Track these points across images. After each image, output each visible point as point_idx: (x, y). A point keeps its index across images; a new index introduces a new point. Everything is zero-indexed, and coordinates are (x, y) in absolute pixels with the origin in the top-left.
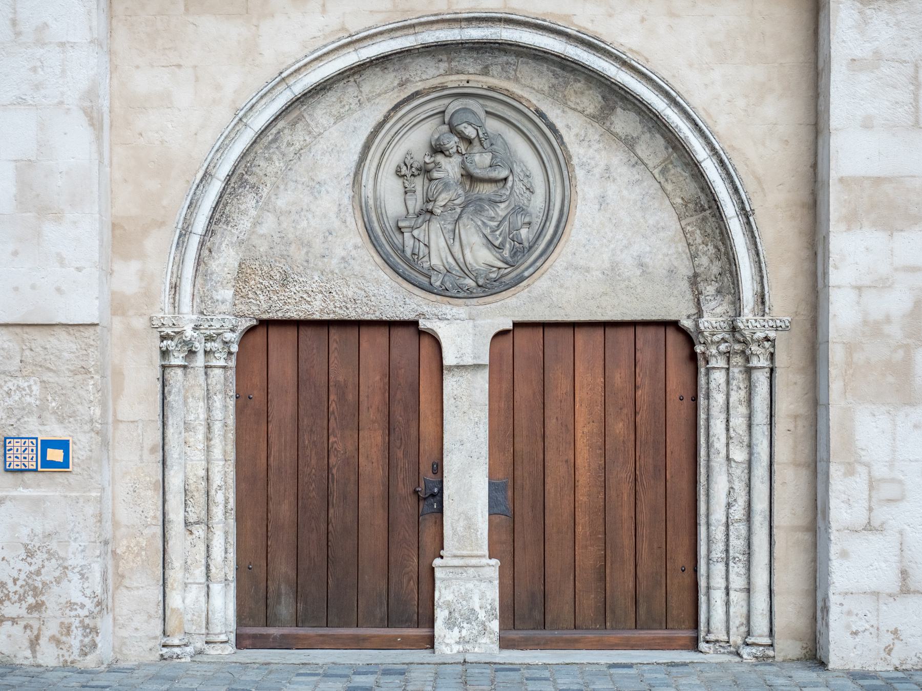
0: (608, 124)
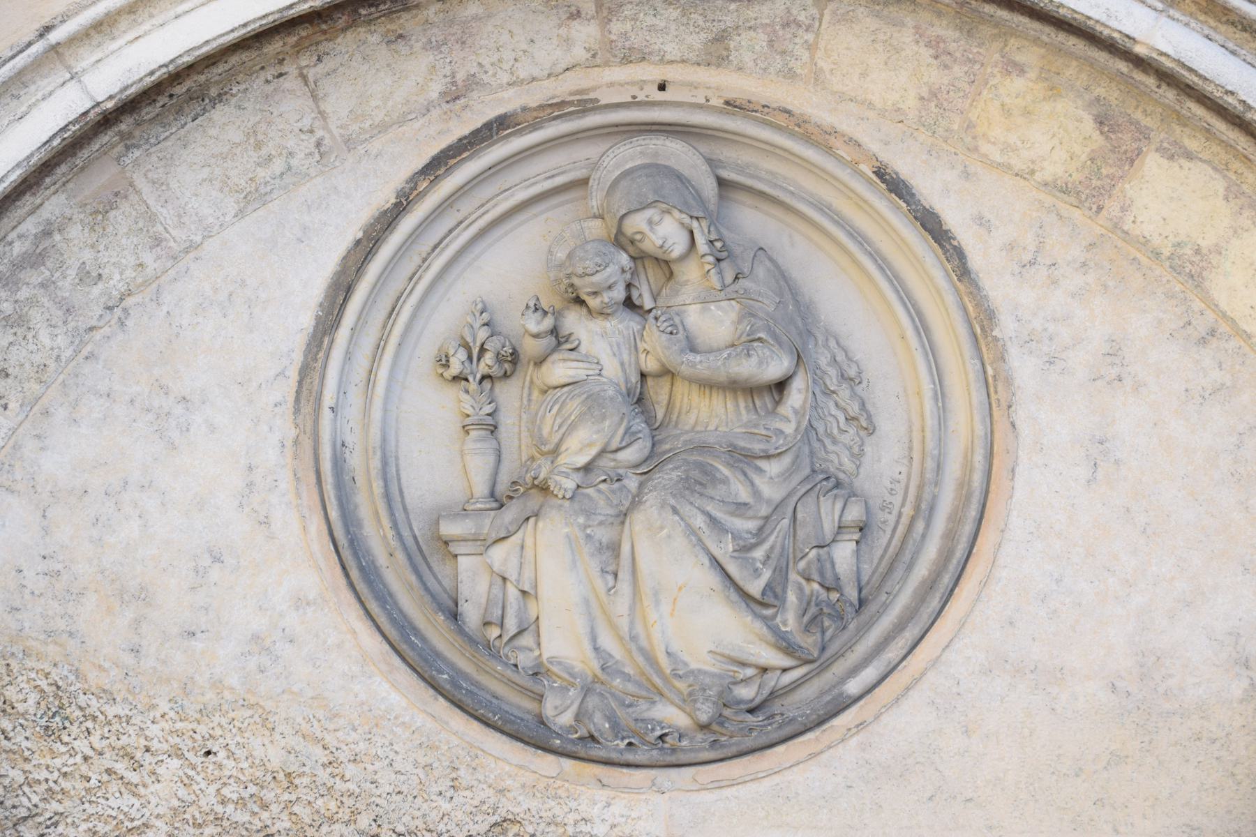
0: (1112, 208)
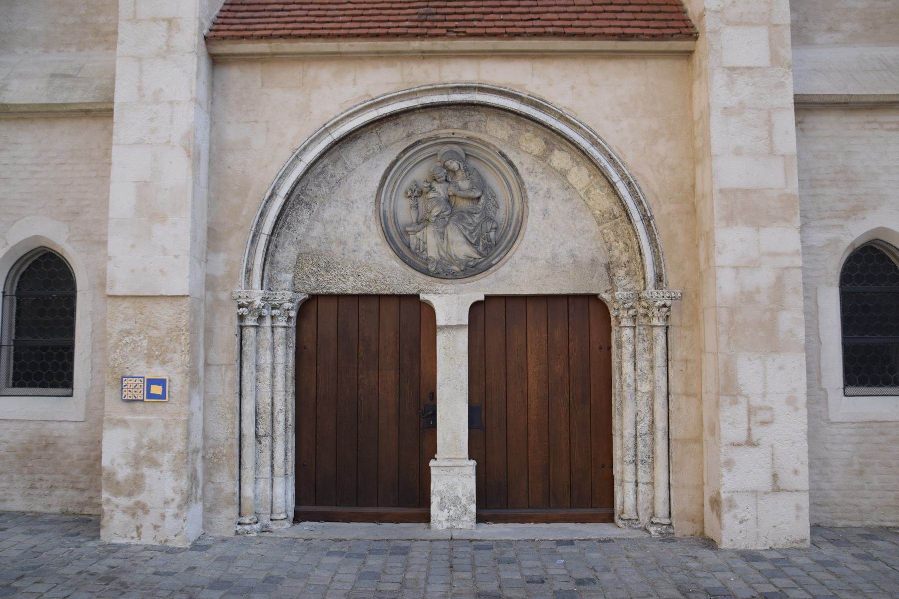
0: (548, 161)
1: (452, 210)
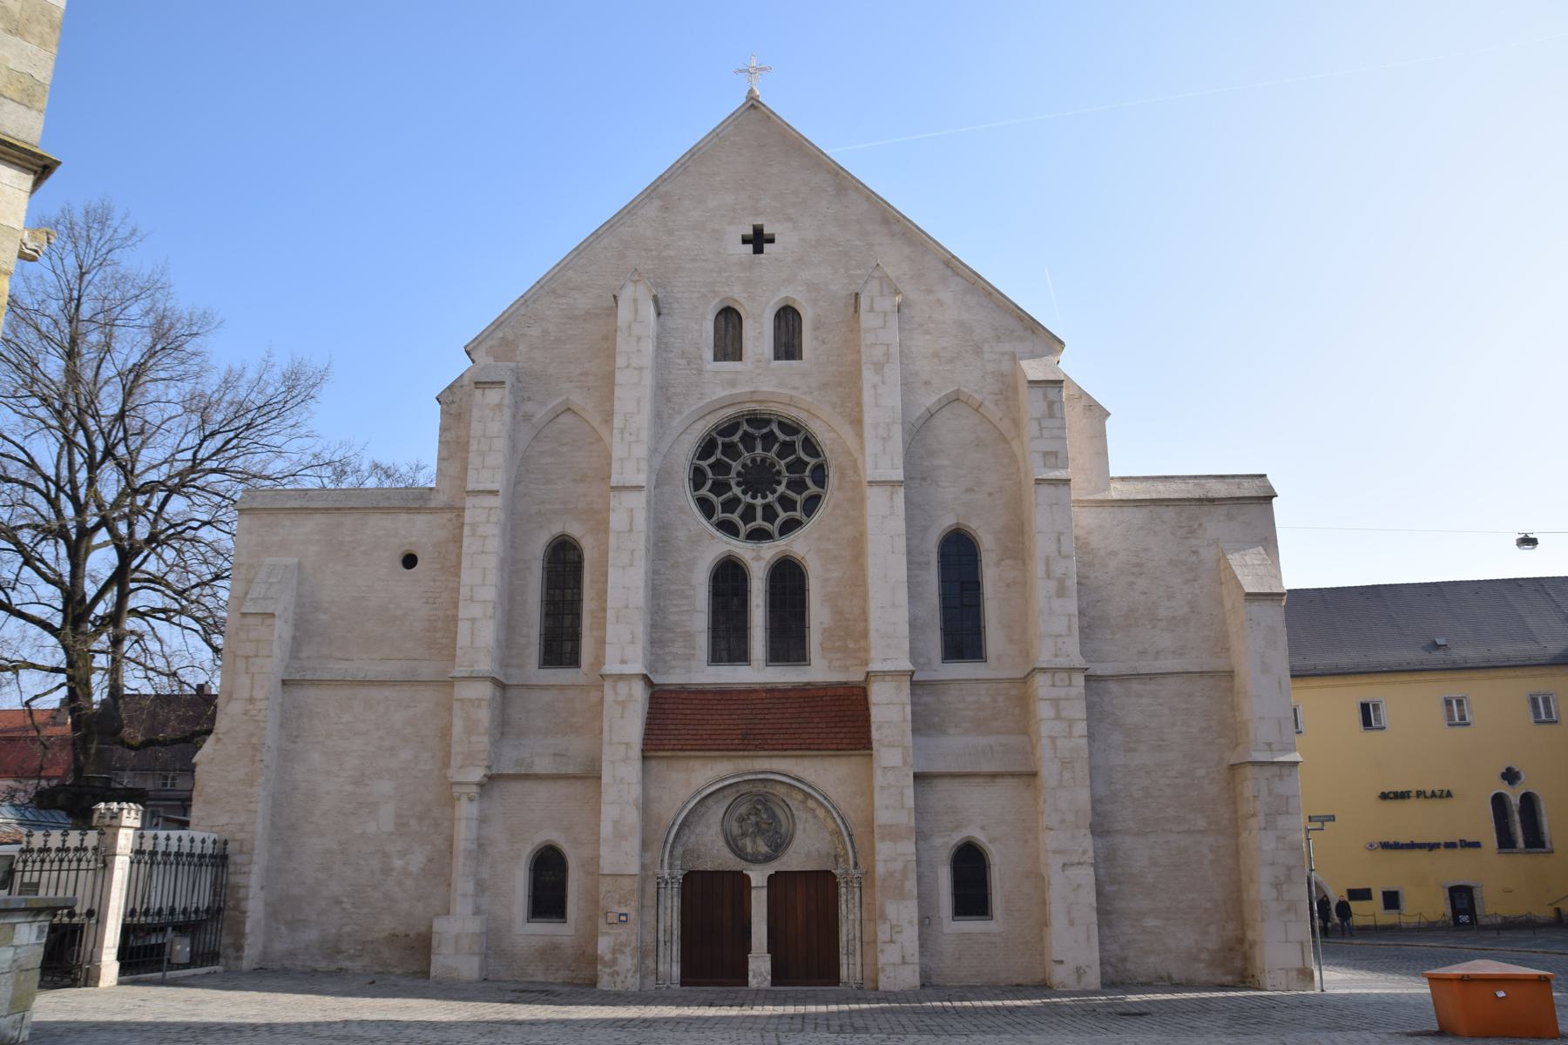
1: (759, 830)
